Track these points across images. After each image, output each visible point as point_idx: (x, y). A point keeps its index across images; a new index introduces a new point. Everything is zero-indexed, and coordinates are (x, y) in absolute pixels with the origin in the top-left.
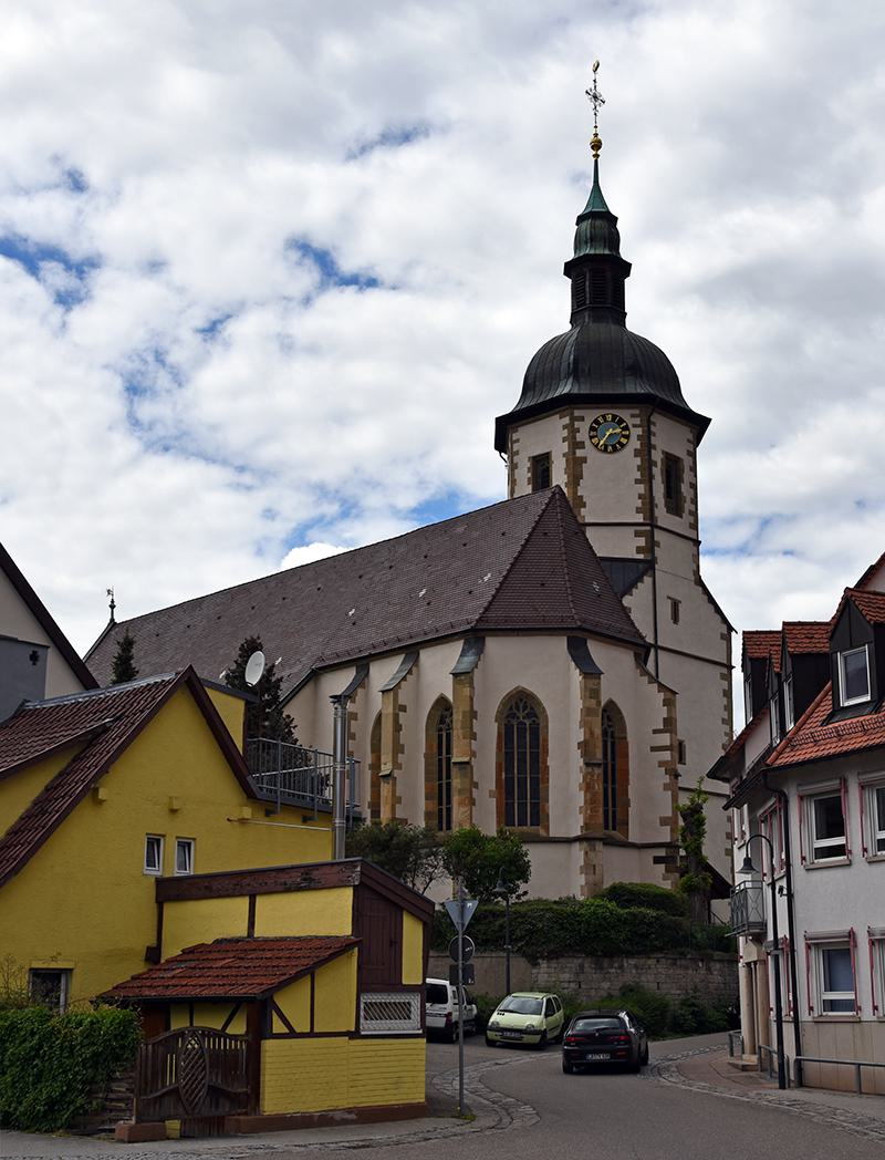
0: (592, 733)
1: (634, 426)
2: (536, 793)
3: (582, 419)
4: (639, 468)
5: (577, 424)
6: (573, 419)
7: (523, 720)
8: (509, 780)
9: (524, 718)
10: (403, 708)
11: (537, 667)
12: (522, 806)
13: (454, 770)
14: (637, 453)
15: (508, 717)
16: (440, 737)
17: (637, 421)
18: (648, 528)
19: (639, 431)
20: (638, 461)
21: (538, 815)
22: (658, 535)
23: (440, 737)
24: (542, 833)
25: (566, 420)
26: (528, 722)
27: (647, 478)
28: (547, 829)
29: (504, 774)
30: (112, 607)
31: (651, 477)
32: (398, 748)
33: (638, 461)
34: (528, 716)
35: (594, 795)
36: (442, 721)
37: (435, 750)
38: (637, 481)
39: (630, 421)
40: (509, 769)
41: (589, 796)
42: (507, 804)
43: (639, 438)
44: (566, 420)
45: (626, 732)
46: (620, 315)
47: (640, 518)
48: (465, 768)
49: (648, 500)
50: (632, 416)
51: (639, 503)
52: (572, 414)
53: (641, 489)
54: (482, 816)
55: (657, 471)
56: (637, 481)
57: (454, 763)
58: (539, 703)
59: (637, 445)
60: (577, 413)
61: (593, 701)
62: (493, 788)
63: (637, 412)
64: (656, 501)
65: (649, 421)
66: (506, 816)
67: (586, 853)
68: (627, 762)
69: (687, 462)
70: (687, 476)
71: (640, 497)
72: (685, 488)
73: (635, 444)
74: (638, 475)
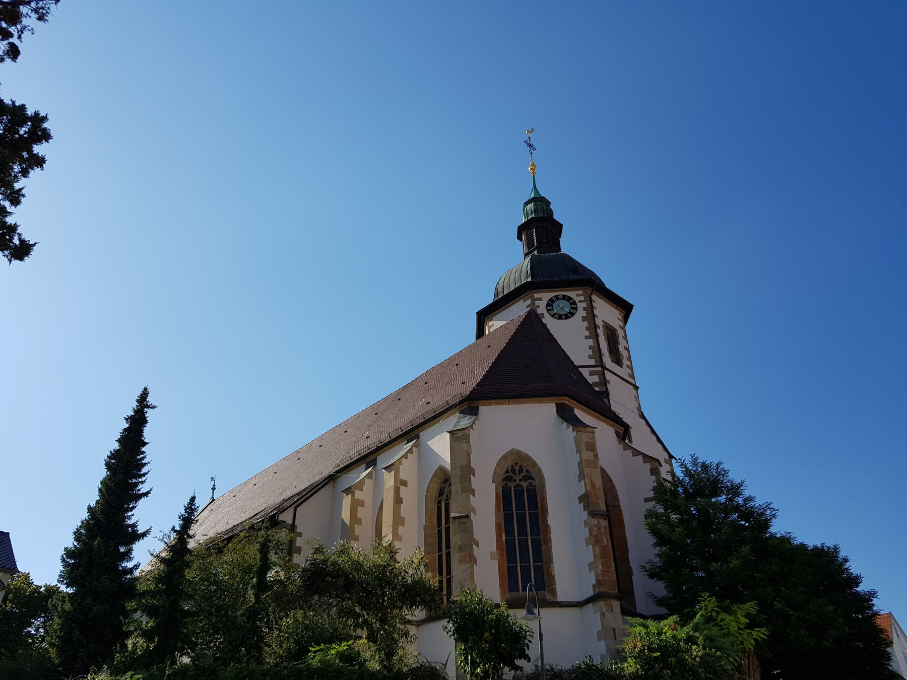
0: (593, 485)
1: (580, 301)
2: (538, 557)
3: (541, 299)
4: (587, 329)
5: (537, 303)
6: (534, 300)
7: (521, 493)
8: (510, 544)
9: (520, 480)
10: (404, 483)
11: (526, 427)
12: (526, 570)
13: (453, 526)
14: (584, 319)
15: (504, 480)
16: (439, 509)
17: (582, 298)
18: (600, 369)
19: (584, 305)
20: (586, 324)
21: (543, 580)
22: (608, 375)
23: (439, 509)
24: (549, 597)
25: (529, 302)
26: (525, 484)
27: (594, 335)
28: (553, 592)
29: (504, 535)
30: (213, 489)
31: (597, 336)
32: (398, 521)
33: (586, 324)
34: (525, 478)
35: (604, 548)
36: (441, 493)
37: (435, 522)
38: (587, 338)
39: (577, 299)
40: (509, 532)
41: (598, 549)
42: (509, 568)
43: (584, 309)
44: (529, 302)
45: (618, 501)
46: (558, 248)
47: (592, 362)
48: (464, 523)
49: (597, 350)
50: (578, 295)
51: (590, 352)
52: (533, 297)
53: (591, 342)
54: (484, 578)
55: (600, 332)
56: (587, 338)
57: (454, 518)
58: (534, 464)
59: (584, 314)
60: (536, 296)
61: (591, 454)
62: (494, 549)
63: (581, 292)
64: (603, 352)
65: (590, 298)
66: (510, 580)
67: (603, 614)
68: (624, 529)
69: (620, 333)
70: (621, 341)
71: (590, 347)
72: (621, 348)
73: (581, 312)
74: (587, 333)
